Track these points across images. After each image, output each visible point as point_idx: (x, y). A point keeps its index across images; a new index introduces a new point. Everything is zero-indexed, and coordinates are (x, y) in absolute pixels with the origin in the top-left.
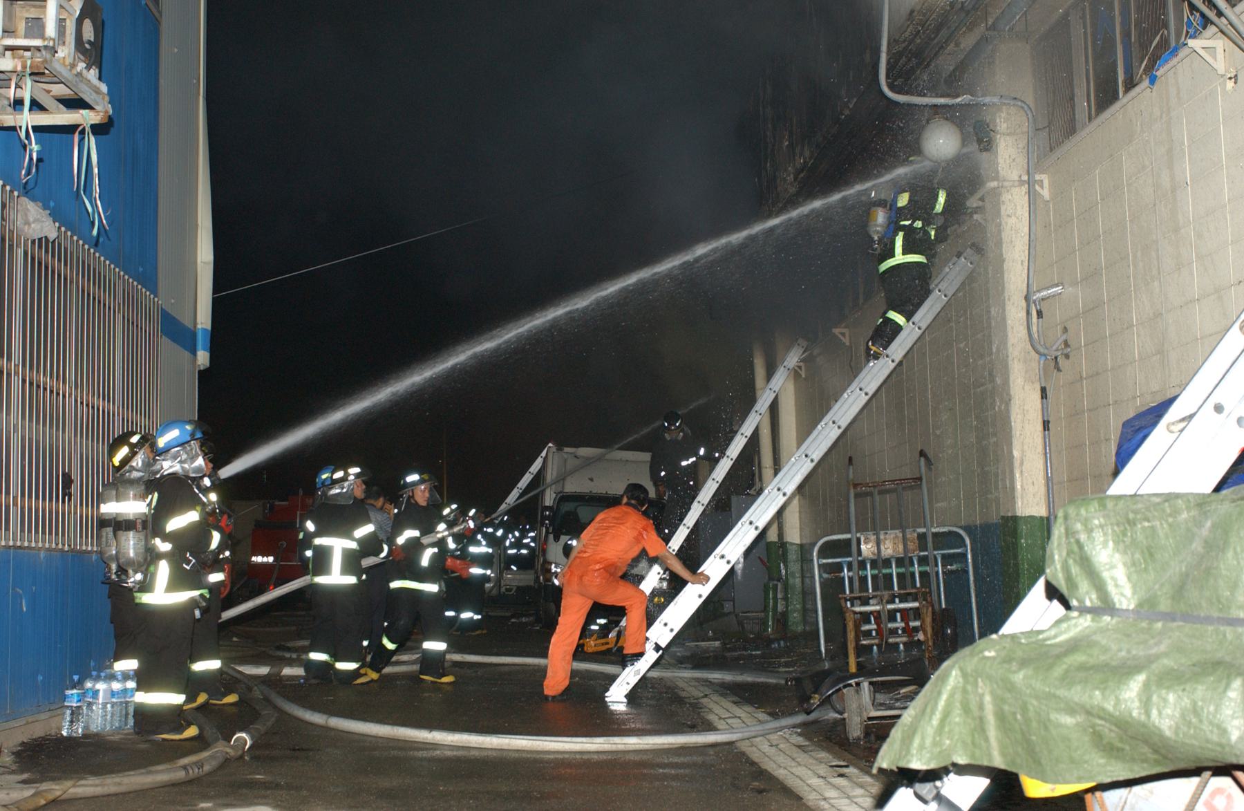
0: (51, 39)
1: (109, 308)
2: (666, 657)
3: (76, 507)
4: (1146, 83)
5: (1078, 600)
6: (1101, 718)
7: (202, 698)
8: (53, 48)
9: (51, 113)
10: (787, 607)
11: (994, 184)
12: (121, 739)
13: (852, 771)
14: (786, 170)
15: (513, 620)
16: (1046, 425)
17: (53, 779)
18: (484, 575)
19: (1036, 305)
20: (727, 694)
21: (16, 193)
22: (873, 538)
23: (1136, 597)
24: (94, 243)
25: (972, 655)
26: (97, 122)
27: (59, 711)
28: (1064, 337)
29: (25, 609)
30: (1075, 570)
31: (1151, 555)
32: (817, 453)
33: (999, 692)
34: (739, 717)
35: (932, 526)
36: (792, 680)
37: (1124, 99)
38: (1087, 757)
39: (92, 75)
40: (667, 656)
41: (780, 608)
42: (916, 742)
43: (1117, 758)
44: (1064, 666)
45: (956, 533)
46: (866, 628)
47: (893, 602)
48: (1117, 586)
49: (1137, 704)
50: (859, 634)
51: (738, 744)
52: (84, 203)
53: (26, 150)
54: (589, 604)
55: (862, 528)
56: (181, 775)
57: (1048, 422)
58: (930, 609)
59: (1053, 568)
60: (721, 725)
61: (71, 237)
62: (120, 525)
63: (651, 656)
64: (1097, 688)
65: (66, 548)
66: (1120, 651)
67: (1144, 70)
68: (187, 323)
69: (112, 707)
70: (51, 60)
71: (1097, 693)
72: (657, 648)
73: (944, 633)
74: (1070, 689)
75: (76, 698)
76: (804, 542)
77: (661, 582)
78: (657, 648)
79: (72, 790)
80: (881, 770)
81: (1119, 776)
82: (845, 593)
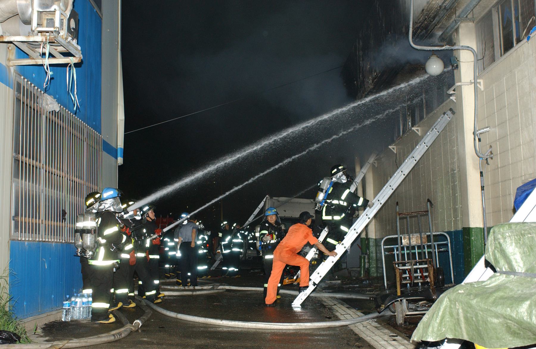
0: (57, 28)
2: (318, 287)
4: (525, 40)
5: (499, 268)
6: (510, 320)
7: (120, 305)
8: (58, 31)
9: (57, 58)
10: (370, 266)
11: (459, 84)
12: (87, 322)
13: (399, 338)
14: (368, 78)
15: (252, 271)
16: (483, 188)
17: (59, 340)
18: (240, 252)
19: (478, 136)
20: (344, 304)
21: (42, 92)
22: (407, 237)
23: (525, 267)
24: (74, 112)
25: (453, 292)
26: (77, 62)
27: (61, 310)
28: (490, 150)
29: (46, 267)
30: (498, 255)
31: (532, 249)
33: (465, 308)
34: (350, 314)
35: (433, 232)
36: (372, 297)
37: (516, 47)
38: (504, 337)
39: (74, 42)
40: (318, 288)
41: (367, 266)
42: (430, 329)
43: (517, 337)
44: (494, 297)
46: (404, 276)
47: (416, 265)
48: (516, 262)
49: (526, 314)
50: (402, 279)
51: (349, 326)
52: (71, 96)
53: (47, 75)
54: (284, 265)
55: (402, 233)
56: (112, 338)
57: (484, 187)
58: (432, 268)
59: (488, 254)
60: (342, 317)
61: (65, 110)
62: (83, 232)
63: (311, 288)
64: (508, 307)
65: (64, 241)
66: (518, 291)
67: (525, 34)
68: (114, 145)
69: (83, 309)
70: (57, 36)
71: (508, 309)
72: (314, 284)
73: (438, 279)
74: (496, 307)
75: (68, 305)
76: (377, 238)
77: (315, 255)
78: (314, 284)
79: (67, 345)
80: (413, 341)
81: (518, 345)
82: (395, 261)
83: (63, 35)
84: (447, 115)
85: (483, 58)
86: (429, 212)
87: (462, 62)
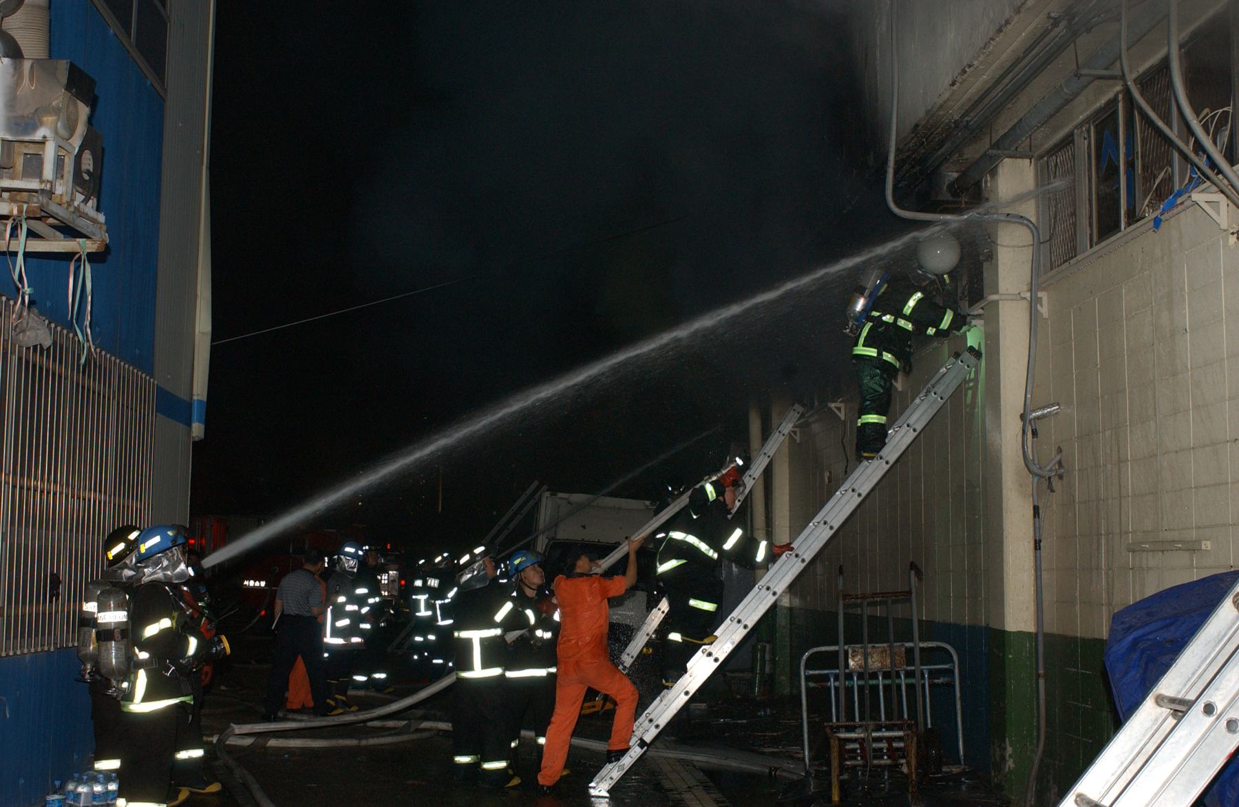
0: (48, 181)
1: (104, 397)
3: (63, 605)
9: (47, 240)
11: (994, 297)
16: (1037, 545)
26: (94, 251)
28: (1058, 458)
29: (8, 715)
32: (808, 552)
39: (90, 208)
41: (767, 670)
45: (944, 648)
57: (1040, 541)
68: (183, 395)
72: (642, 743)
78: (642, 743)
82: (831, 721)
83: (61, 195)
84: (962, 362)
85: (1050, 239)
86: (914, 595)
87: (1002, 246)
